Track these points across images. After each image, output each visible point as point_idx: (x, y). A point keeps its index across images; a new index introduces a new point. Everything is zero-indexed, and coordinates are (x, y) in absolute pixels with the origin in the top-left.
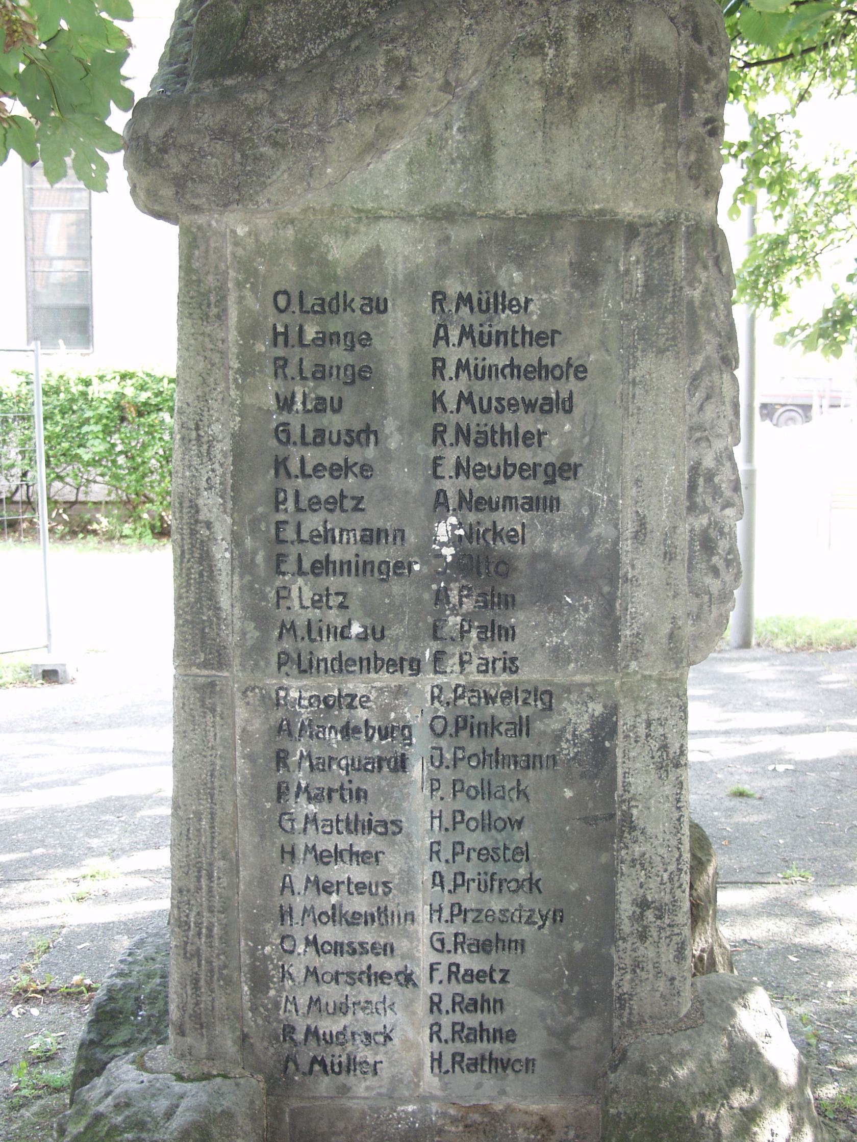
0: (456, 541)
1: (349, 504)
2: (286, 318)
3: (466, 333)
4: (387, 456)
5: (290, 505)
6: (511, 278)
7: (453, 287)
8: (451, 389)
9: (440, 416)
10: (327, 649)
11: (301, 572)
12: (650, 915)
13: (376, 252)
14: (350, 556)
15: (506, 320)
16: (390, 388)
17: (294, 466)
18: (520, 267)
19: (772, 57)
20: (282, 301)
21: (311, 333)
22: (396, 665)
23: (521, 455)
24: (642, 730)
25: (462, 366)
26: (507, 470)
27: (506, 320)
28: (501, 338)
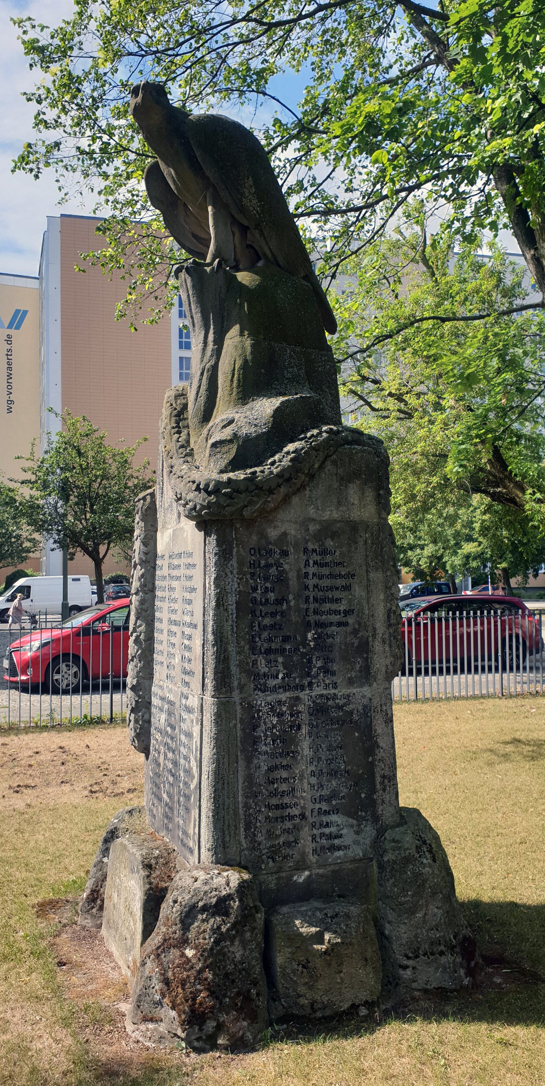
0: (314, 639)
1: (277, 627)
2: (253, 558)
3: (315, 563)
4: (289, 608)
5: (257, 628)
6: (330, 543)
7: (310, 546)
8: (311, 582)
9: (307, 593)
10: (272, 683)
11: (261, 653)
12: (386, 781)
13: (285, 534)
14: (278, 647)
15: (328, 558)
16: (291, 583)
17: (258, 613)
18: (333, 539)
19: (367, 407)
20: (252, 552)
21: (263, 562)
22: (296, 687)
23: (334, 607)
24: (379, 708)
25: (314, 575)
26: (330, 612)
27: (328, 558)
28: (326, 565)
